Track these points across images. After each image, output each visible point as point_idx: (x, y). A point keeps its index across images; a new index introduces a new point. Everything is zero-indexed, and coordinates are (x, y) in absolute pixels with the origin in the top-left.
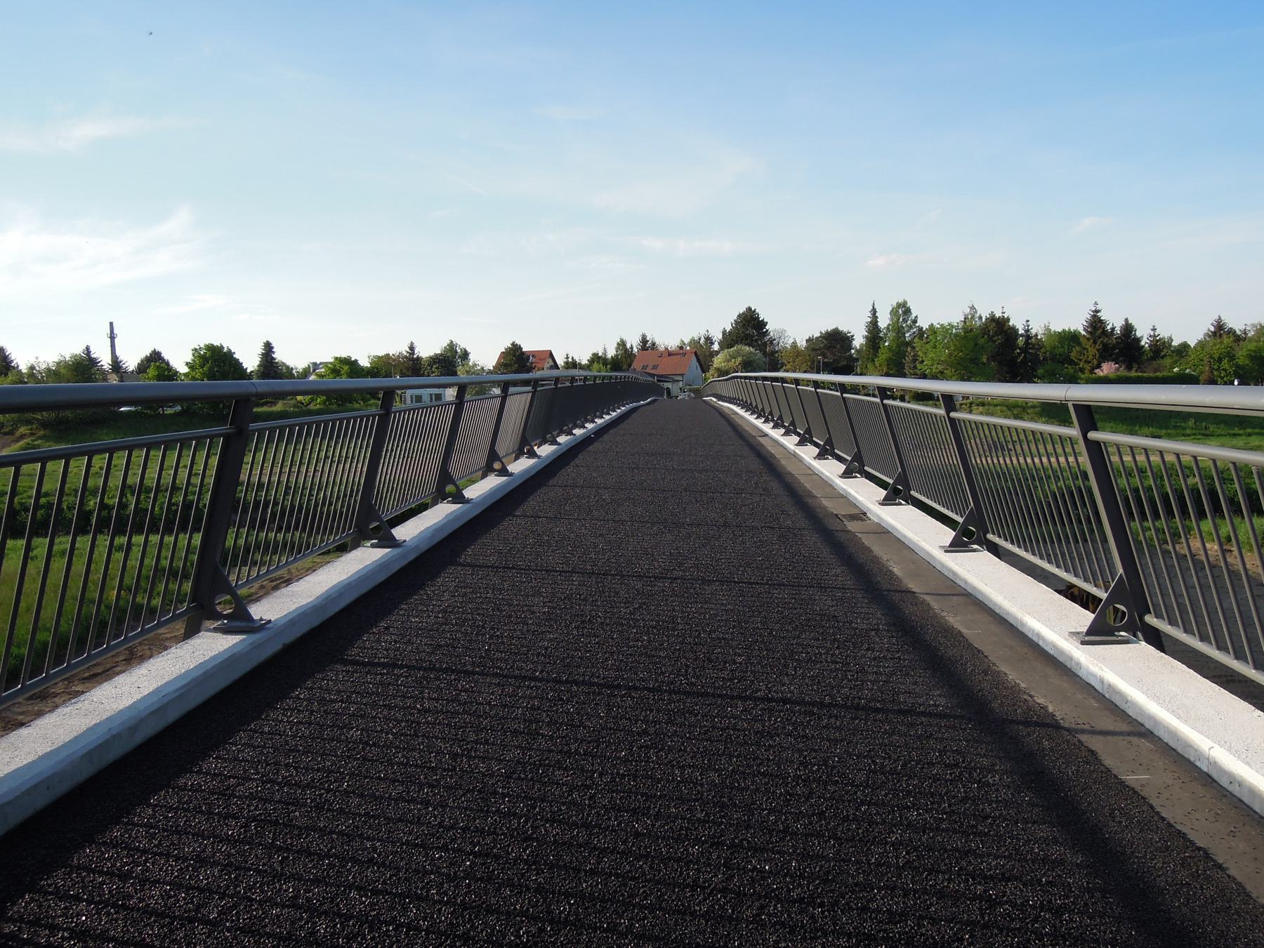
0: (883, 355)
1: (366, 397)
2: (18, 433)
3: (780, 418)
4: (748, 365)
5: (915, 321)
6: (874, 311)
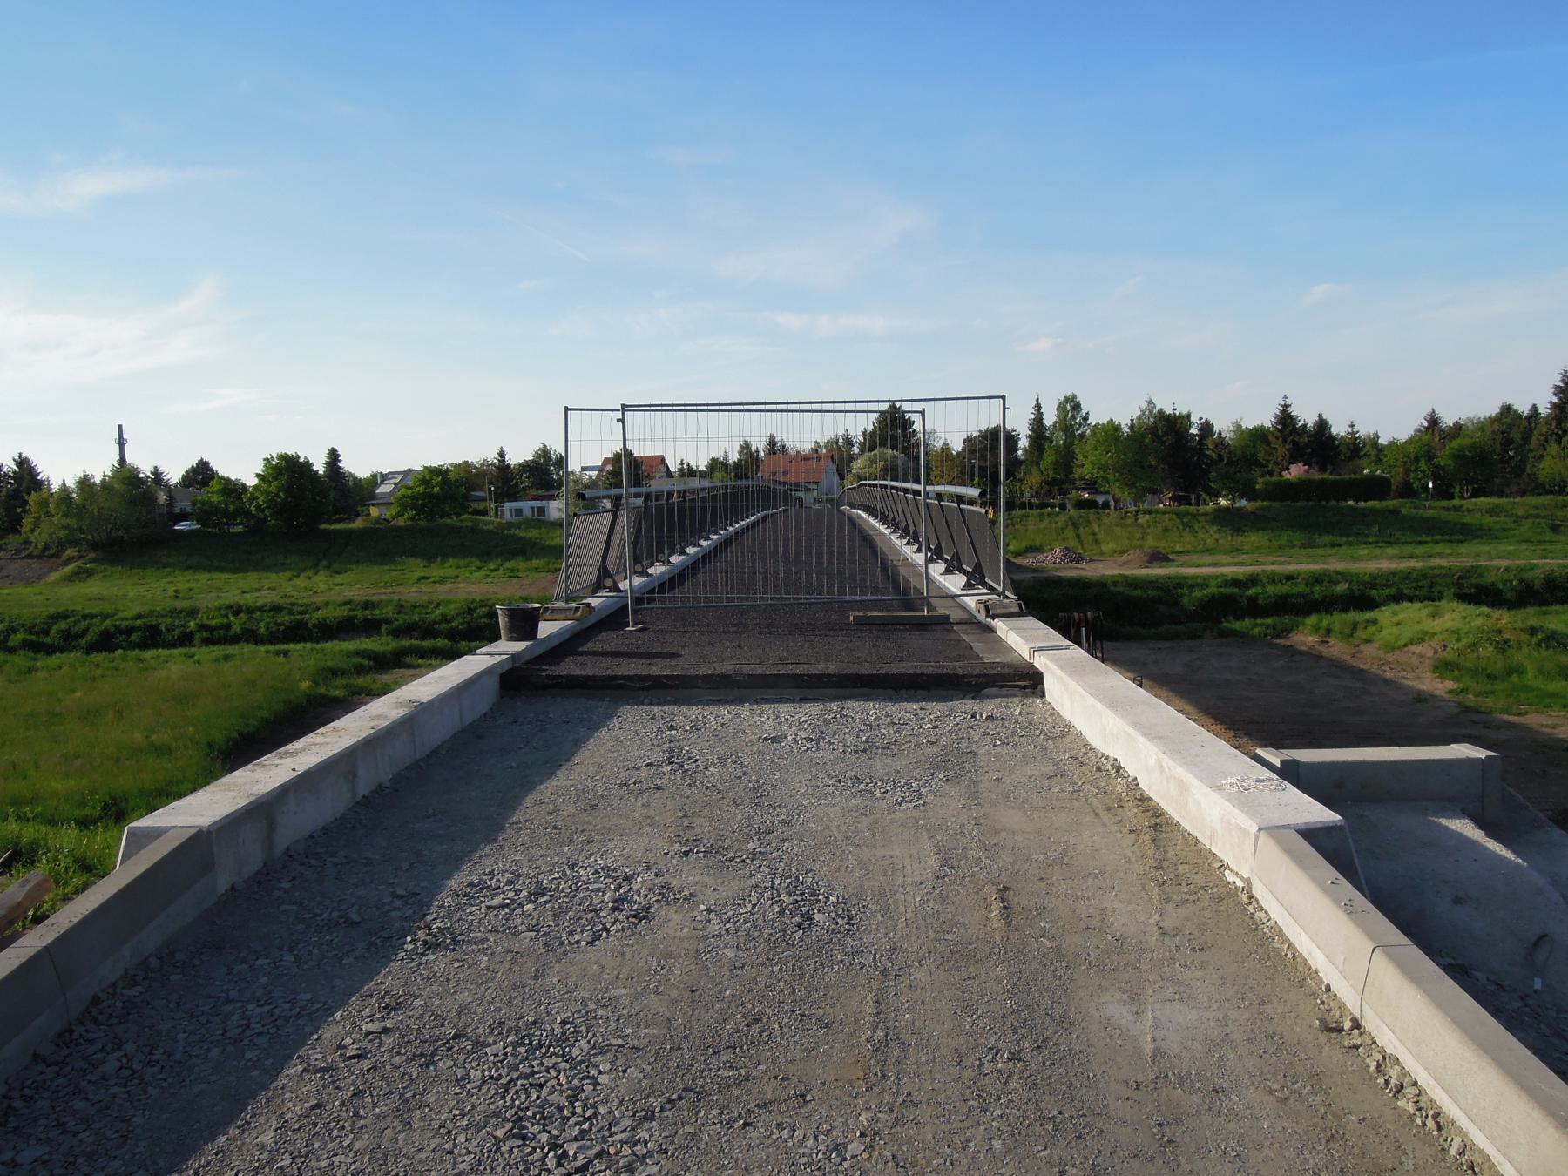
1: (453, 509)
2: (65, 556)
3: (939, 547)
4: (892, 472)
5: (1086, 418)
6: (1038, 407)
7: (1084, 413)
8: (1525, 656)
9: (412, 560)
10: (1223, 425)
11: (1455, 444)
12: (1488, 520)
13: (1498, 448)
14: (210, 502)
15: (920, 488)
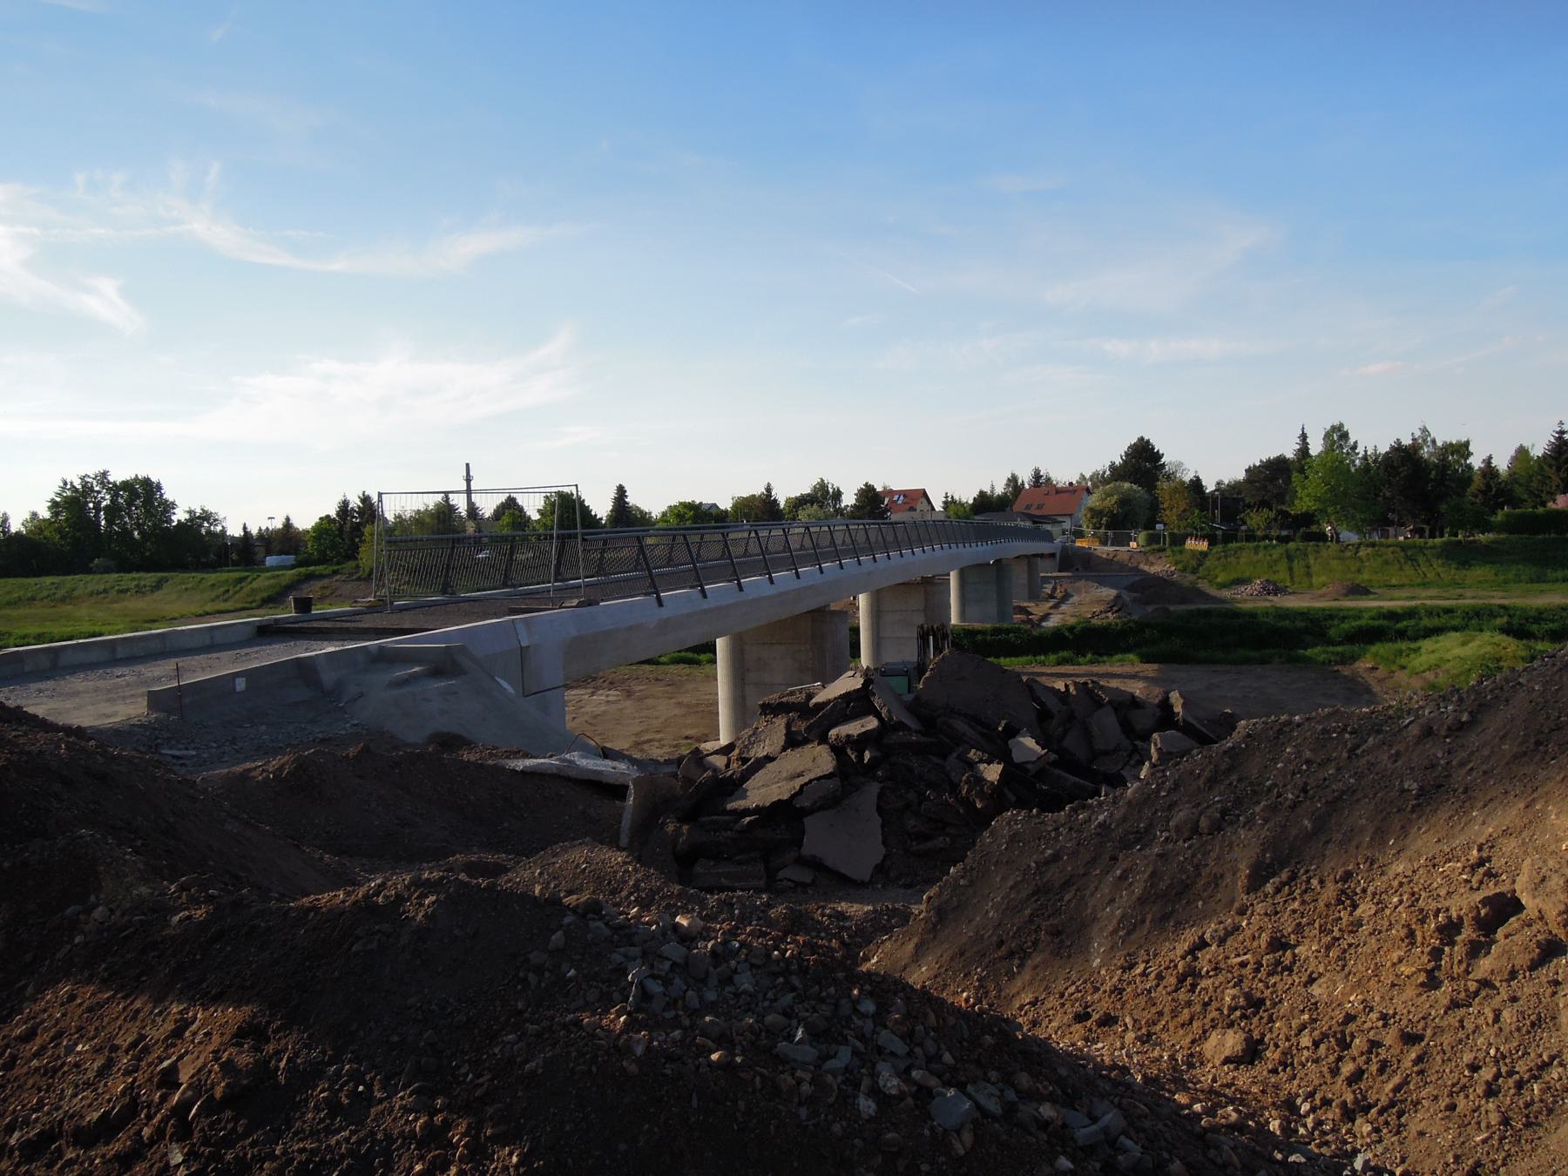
5: (1354, 447)
6: (1304, 437)
7: (1352, 441)
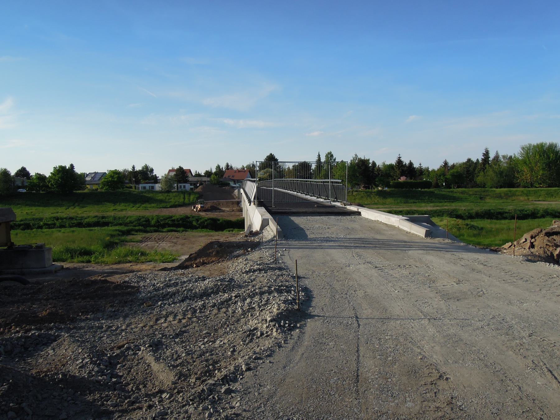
0: (323, 173)
5: (335, 160)
6: (319, 155)
7: (252, 203)
8: (465, 232)
9: (108, 204)
10: (379, 163)
11: (452, 171)
12: (461, 195)
13: (465, 173)
14: (33, 182)
15: (329, 180)
